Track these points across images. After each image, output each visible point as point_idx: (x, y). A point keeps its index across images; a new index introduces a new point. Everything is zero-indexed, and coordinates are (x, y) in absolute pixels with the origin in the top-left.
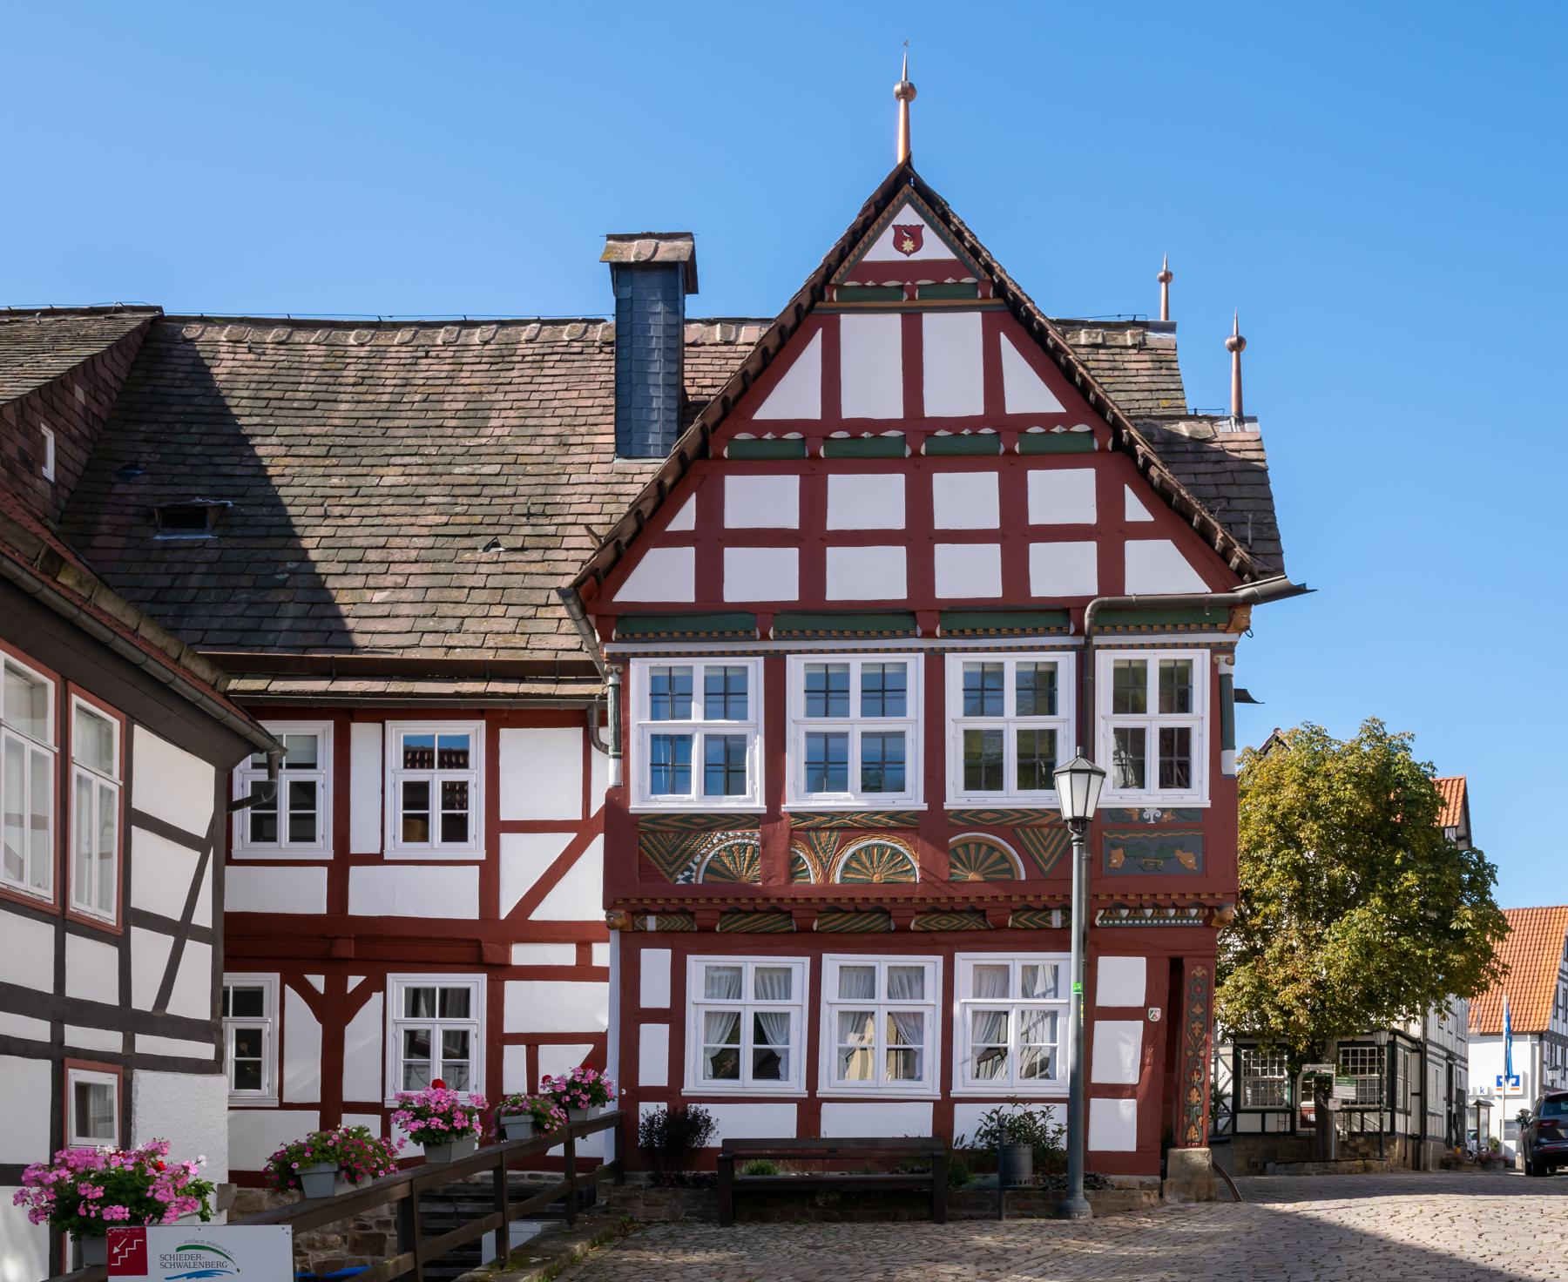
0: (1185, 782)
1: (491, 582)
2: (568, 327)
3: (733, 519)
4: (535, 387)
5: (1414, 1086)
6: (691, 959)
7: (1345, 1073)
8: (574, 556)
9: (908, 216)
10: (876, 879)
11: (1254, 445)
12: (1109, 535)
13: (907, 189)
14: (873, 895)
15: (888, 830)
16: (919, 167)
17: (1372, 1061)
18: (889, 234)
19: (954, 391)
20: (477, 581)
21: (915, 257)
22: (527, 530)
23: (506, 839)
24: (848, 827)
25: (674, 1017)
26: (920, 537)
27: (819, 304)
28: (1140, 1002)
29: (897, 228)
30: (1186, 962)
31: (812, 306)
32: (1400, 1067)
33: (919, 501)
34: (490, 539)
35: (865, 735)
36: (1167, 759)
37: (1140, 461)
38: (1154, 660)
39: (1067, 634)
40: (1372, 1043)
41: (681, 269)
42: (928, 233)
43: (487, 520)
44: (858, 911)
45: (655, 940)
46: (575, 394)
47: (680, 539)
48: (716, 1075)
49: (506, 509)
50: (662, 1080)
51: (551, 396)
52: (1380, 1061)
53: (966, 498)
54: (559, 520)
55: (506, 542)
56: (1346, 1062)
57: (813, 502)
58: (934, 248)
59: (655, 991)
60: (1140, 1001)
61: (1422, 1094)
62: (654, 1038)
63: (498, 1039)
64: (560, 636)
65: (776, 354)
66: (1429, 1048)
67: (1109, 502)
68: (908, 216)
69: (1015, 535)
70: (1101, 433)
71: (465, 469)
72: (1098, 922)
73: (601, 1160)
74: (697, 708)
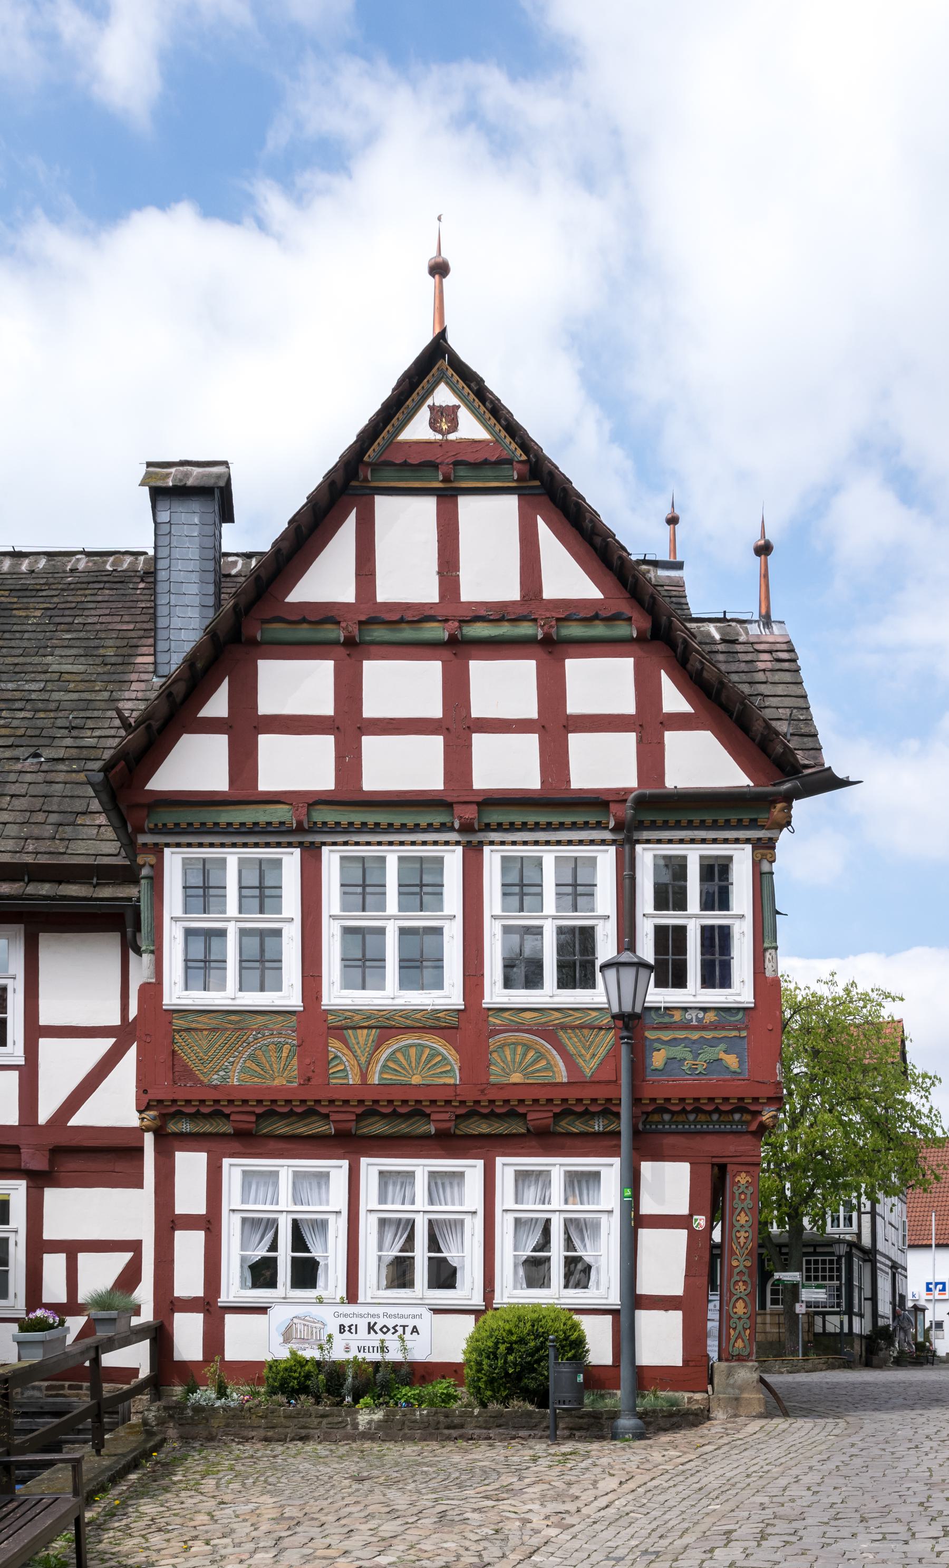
0: (725, 982)
1: (34, 790)
2: (111, 559)
3: (267, 705)
4: (79, 612)
5: (867, 1293)
6: (226, 1162)
7: (808, 1278)
8: (108, 739)
9: (443, 396)
10: (416, 1080)
11: (784, 647)
12: (648, 725)
13: (444, 363)
14: (412, 1096)
15: (424, 1029)
16: (454, 341)
17: (831, 1270)
18: (424, 415)
19: (490, 578)
20: (22, 789)
21: (452, 437)
22: (69, 742)
23: (44, 1043)
24: (388, 1026)
25: (210, 1223)
26: (457, 726)
27: (353, 483)
28: (685, 1211)
29: (432, 408)
30: (729, 1167)
31: (346, 485)
32: (856, 1275)
33: (456, 690)
34: (32, 750)
35: (403, 931)
36: (708, 957)
37: (680, 648)
38: (694, 856)
39: (606, 828)
40: (832, 1254)
41: (217, 492)
42: (464, 415)
43: (29, 732)
44: (395, 1115)
45: (192, 1141)
46: (118, 619)
47: (213, 726)
48: (255, 1285)
49: (48, 723)
50: (198, 1290)
51: (95, 619)
52: (839, 1270)
53: (504, 686)
54: (97, 733)
55: (47, 753)
56: (808, 1270)
57: (349, 689)
58: (470, 428)
59: (190, 1198)
60: (683, 1209)
61: (874, 1299)
62: (189, 1247)
63: (38, 1246)
64: (98, 842)
65: (309, 535)
66: (878, 1257)
67: (647, 692)
68: (443, 396)
69: (554, 725)
70: (643, 610)
71: (10, 686)
72: (641, 1127)
73: (136, 1371)
74: (232, 908)
